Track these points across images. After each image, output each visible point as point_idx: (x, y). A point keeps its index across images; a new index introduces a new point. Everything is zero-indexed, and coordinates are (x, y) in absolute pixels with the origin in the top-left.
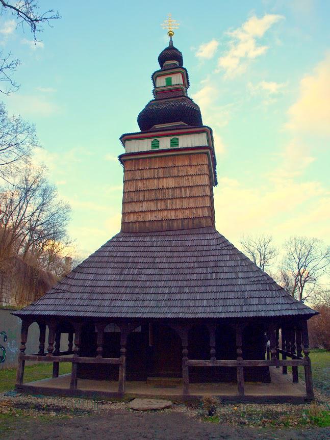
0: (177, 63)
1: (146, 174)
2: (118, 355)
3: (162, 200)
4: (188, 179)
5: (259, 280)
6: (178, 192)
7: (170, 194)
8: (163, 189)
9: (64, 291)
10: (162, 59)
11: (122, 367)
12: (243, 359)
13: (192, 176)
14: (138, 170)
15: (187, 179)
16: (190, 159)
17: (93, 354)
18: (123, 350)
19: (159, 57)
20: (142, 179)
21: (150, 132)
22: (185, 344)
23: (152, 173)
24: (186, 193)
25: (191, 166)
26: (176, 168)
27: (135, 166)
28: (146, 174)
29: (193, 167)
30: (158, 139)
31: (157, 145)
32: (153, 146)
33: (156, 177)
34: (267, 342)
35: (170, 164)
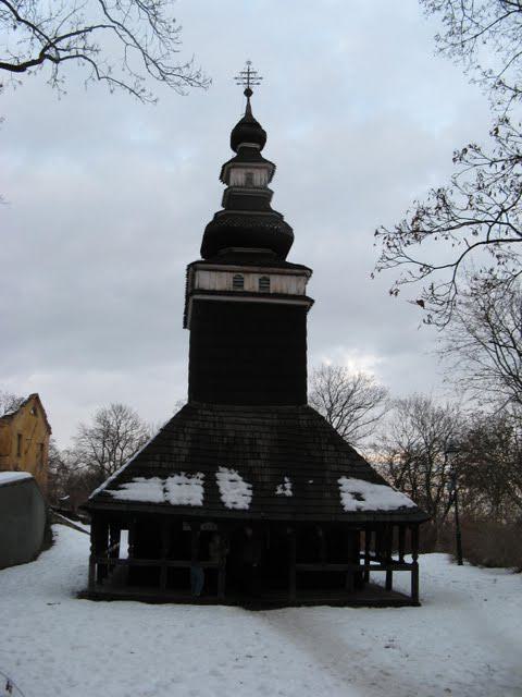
19: (209, 228)
20: (214, 422)
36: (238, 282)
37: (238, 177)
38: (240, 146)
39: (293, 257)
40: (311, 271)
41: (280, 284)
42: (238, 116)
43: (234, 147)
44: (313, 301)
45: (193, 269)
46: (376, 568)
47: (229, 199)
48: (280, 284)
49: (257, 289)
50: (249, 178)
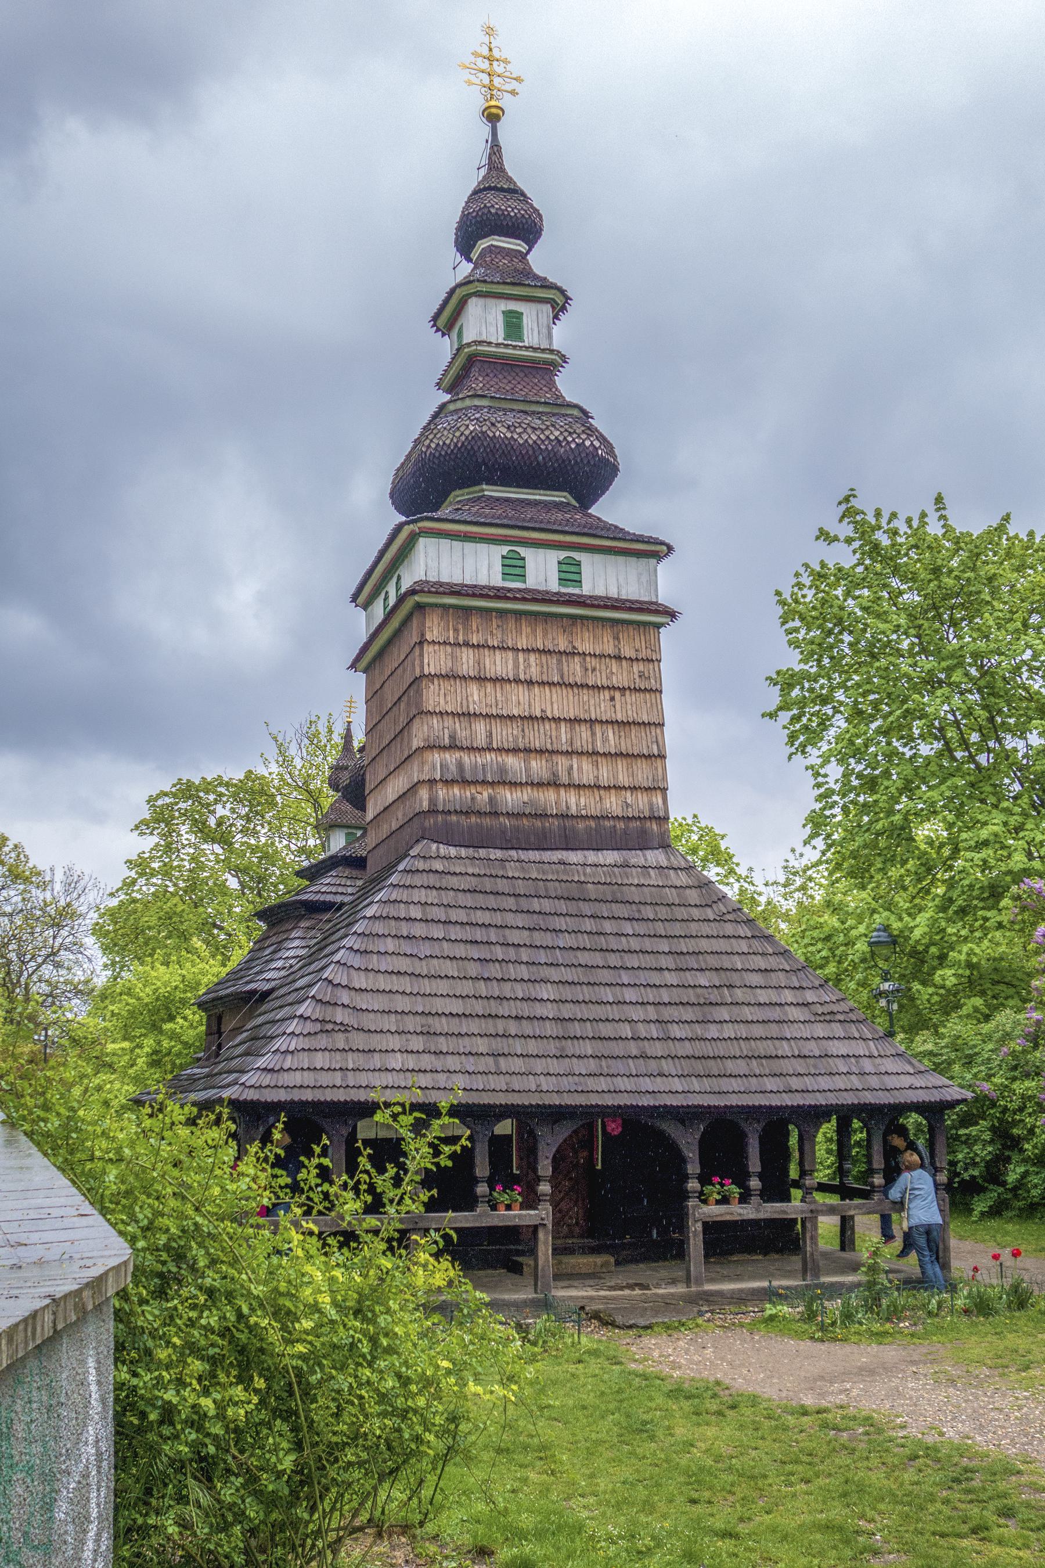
0: (522, 247)
1: (499, 664)
2: (531, 1201)
3: (541, 752)
4: (612, 699)
5: (644, 1056)
6: (584, 735)
7: (563, 736)
8: (543, 719)
9: (345, 1028)
10: (471, 231)
11: (546, 1234)
13: (622, 690)
14: (466, 644)
15: (608, 697)
16: (617, 638)
17: (468, 1202)
18: (545, 1188)
20: (481, 679)
21: (439, 520)
22: (693, 1168)
23: (511, 662)
24: (605, 740)
25: (618, 658)
26: (577, 659)
27: (456, 630)
28: (499, 664)
29: (624, 662)
30: (522, 551)
31: (517, 571)
32: (508, 570)
33: (522, 677)
34: (651, 1232)
35: (563, 645)
36: (514, 566)
37: (484, 323)
38: (483, 244)
41: (603, 577)
43: (465, 244)
48: (603, 577)
49: (554, 586)
50: (513, 324)
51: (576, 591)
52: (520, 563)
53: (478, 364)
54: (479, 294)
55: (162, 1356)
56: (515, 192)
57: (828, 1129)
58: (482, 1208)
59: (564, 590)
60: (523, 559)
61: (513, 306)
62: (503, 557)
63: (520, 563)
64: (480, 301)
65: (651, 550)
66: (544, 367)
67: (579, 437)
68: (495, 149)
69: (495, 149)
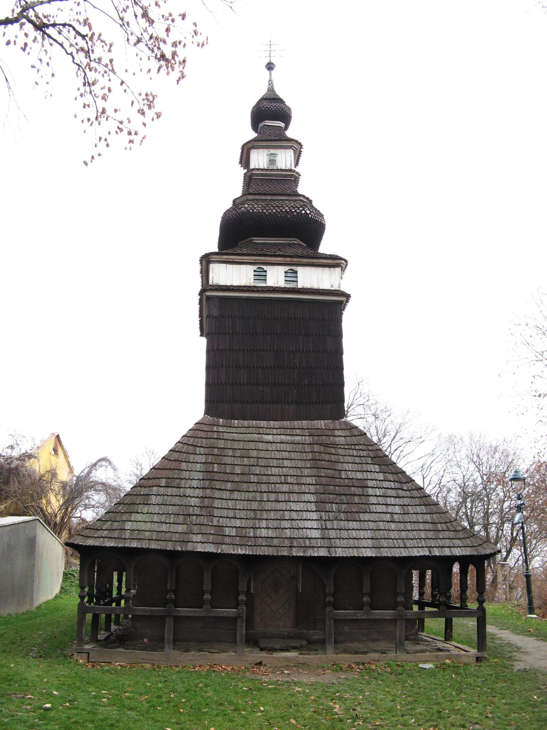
0: (282, 125)
11: (242, 623)
12: (447, 609)
30: (265, 268)
31: (263, 278)
37: (259, 159)
38: (261, 125)
39: (324, 248)
40: (348, 296)
41: (310, 278)
42: (262, 92)
44: (348, 296)
45: (206, 260)
46: (432, 615)
47: (253, 181)
48: (310, 278)
51: (263, 285)
52: (264, 274)
53: (254, 181)
54: (254, 147)
55: (535, 526)
56: (279, 100)
57: (456, 568)
58: (207, 606)
59: (288, 286)
60: (266, 271)
61: (272, 151)
62: (255, 271)
63: (264, 274)
64: (255, 151)
65: (335, 262)
66: (290, 179)
67: (299, 209)
68: (271, 82)
69: (271, 82)
